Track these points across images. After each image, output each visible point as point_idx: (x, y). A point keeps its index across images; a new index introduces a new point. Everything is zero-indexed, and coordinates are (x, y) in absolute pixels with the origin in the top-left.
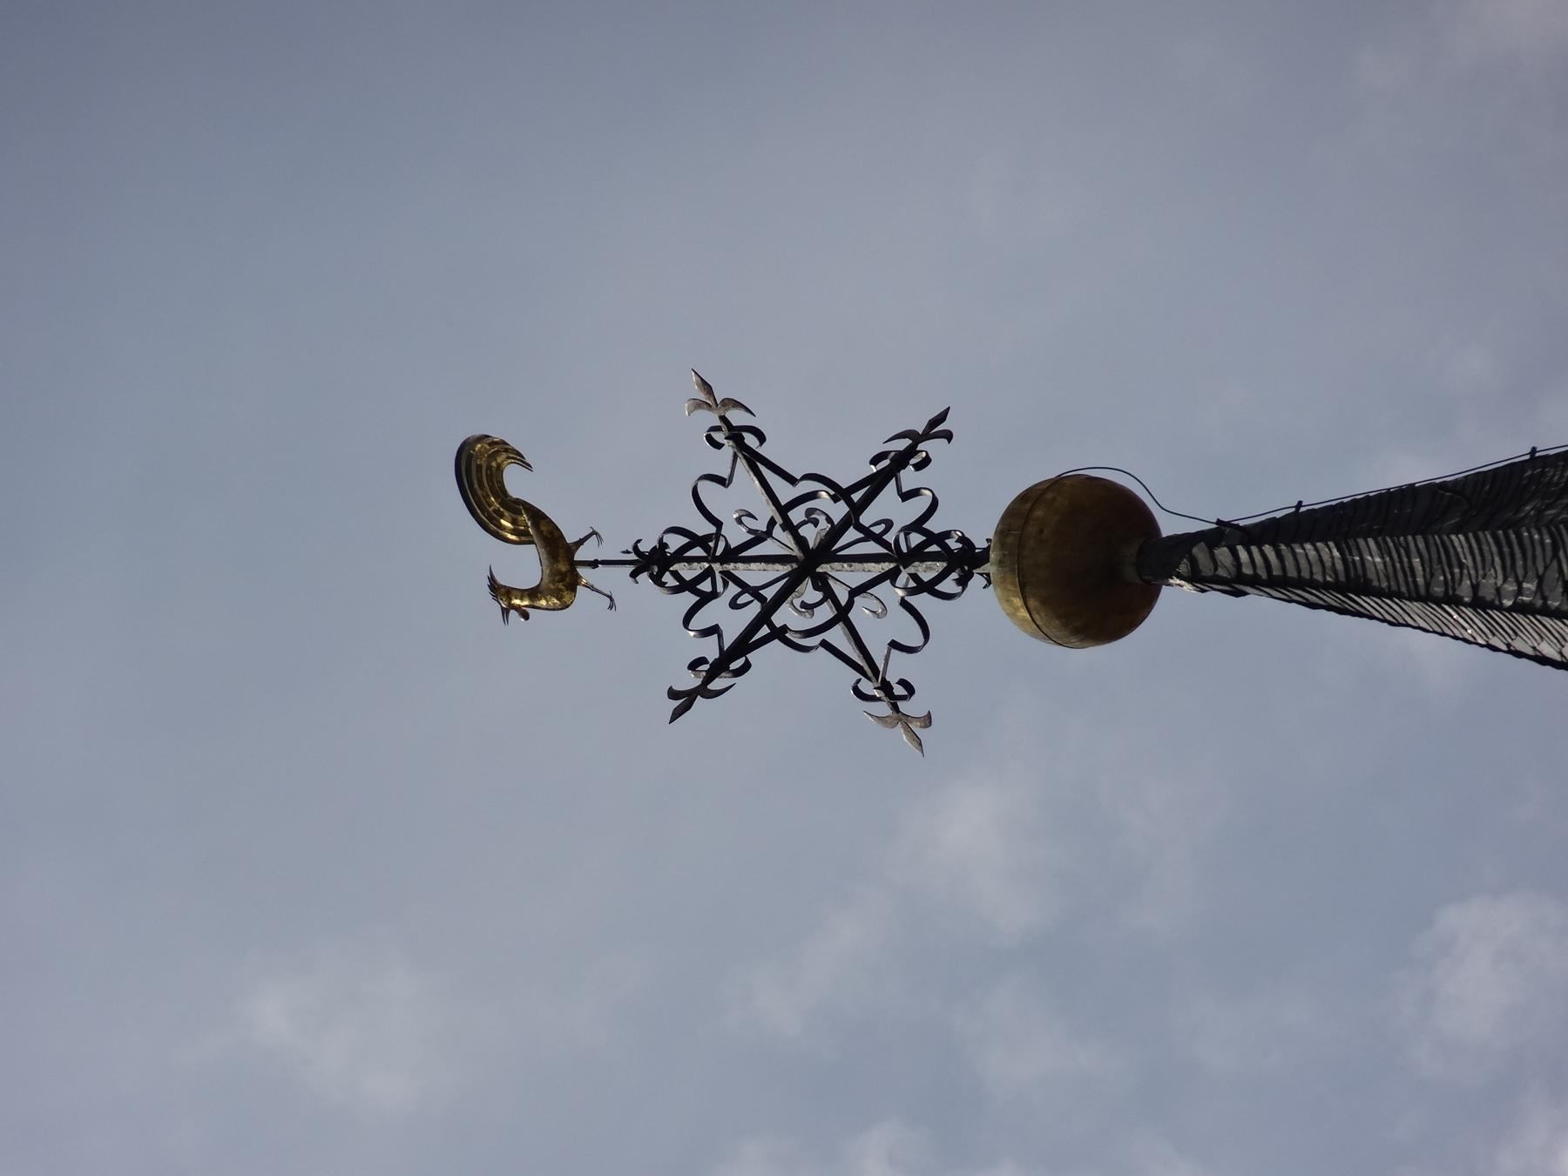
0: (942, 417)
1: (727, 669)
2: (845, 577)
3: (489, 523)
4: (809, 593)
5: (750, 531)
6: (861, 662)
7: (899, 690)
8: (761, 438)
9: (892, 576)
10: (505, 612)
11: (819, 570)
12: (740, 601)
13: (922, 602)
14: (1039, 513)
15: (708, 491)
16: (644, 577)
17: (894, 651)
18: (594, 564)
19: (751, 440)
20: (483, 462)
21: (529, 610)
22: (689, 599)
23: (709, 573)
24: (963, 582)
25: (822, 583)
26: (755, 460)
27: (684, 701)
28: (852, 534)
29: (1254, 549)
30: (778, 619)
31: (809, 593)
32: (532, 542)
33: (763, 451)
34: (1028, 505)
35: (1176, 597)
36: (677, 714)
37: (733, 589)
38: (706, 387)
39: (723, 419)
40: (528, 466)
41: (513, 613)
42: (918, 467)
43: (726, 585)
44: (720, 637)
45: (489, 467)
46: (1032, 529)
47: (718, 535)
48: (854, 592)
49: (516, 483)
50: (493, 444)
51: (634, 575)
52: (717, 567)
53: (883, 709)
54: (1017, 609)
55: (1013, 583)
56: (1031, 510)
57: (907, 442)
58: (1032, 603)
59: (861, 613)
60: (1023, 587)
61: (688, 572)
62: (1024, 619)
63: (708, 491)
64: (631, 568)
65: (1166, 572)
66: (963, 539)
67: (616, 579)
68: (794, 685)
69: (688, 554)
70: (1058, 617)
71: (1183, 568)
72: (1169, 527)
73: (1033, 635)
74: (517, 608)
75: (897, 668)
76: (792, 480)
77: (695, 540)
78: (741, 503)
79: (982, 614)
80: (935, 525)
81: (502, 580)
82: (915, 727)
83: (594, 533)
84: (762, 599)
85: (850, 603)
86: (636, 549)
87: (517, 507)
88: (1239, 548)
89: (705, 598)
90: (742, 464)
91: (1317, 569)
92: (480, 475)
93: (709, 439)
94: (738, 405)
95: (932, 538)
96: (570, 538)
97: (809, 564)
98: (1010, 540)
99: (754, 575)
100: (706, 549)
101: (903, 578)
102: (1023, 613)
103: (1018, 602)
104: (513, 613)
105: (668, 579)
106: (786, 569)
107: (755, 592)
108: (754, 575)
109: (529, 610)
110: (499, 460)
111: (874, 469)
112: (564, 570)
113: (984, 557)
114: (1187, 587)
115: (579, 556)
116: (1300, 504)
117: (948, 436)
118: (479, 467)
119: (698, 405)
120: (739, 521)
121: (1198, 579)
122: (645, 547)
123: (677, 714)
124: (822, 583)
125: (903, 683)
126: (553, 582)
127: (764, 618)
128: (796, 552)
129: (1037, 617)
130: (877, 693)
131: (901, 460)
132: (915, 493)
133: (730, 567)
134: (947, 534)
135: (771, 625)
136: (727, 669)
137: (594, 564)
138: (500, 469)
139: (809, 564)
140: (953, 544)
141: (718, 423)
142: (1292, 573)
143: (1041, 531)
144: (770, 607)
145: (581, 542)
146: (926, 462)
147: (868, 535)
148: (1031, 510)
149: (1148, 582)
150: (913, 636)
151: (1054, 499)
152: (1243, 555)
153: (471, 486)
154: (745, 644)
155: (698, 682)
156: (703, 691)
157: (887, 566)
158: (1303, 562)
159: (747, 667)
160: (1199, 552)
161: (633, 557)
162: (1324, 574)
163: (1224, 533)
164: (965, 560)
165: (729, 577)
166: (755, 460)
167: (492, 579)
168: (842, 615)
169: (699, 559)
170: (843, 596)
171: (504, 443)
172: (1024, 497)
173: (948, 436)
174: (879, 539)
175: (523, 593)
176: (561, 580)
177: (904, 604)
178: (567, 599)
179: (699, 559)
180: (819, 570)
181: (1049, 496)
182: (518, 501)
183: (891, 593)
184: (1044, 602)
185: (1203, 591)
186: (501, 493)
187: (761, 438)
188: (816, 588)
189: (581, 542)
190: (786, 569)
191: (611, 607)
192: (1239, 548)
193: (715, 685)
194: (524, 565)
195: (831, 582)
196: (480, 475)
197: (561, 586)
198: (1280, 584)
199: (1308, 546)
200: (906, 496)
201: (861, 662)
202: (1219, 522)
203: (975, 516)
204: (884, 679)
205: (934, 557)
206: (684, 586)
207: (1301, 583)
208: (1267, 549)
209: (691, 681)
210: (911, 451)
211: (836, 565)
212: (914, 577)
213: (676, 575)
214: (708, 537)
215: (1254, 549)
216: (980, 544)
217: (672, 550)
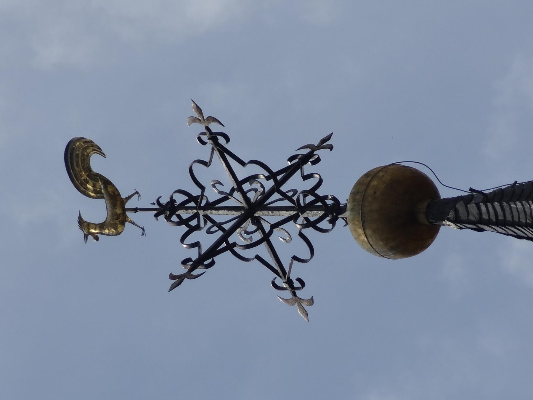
0: (328, 138)
1: (202, 264)
2: (269, 218)
3: (80, 186)
4: (249, 226)
5: (220, 192)
6: (277, 268)
7: (297, 284)
8: (227, 139)
9: (294, 218)
10: (86, 236)
11: (256, 215)
12: (212, 230)
13: (309, 232)
14: (374, 183)
15: (198, 169)
16: (162, 217)
17: (295, 262)
18: (136, 210)
19: (221, 140)
20: (79, 152)
21: (99, 235)
22: (184, 229)
23: (196, 216)
24: (333, 222)
25: (257, 221)
26: (223, 152)
27: (178, 280)
28: (276, 196)
29: (489, 205)
30: (231, 240)
31: (249, 226)
32: (103, 197)
33: (228, 147)
34: (369, 179)
35: (448, 231)
36: (173, 287)
37: (209, 224)
38: (199, 110)
39: (207, 128)
40: (103, 155)
41: (90, 237)
42: (314, 163)
43: (206, 223)
44: (200, 248)
45: (83, 155)
46: (370, 191)
47: (202, 195)
48: (274, 226)
49: (96, 164)
50: (86, 142)
51: (156, 216)
52: (201, 212)
53: (288, 294)
54: (359, 235)
55: (358, 221)
56: (370, 181)
57: (309, 150)
58: (368, 232)
59: (277, 238)
60: (363, 222)
61: (185, 214)
62: (364, 241)
63: (198, 169)
64: (155, 212)
65: (443, 217)
66: (334, 199)
67: (146, 219)
68: (238, 277)
69: (187, 205)
70: (382, 240)
71: (451, 215)
72: (445, 193)
73: (368, 250)
74: (92, 234)
75: (297, 272)
76: (243, 164)
77: (191, 198)
78: (216, 177)
79: (343, 243)
80: (320, 192)
81: (85, 218)
82: (305, 305)
83: (137, 192)
84: (223, 230)
85: (271, 232)
86: (158, 201)
87: (96, 177)
88: (481, 204)
89: (192, 229)
90: (216, 154)
91: (522, 216)
92: (77, 158)
93: (200, 139)
94: (215, 120)
95: (319, 199)
96: (124, 196)
97: (251, 211)
98: (358, 197)
99: (219, 216)
100: (196, 203)
101: (301, 220)
102: (363, 237)
103: (361, 231)
104: (90, 237)
105: (174, 218)
106: (238, 214)
107: (220, 226)
108: (219, 216)
109: (99, 235)
110: (88, 151)
111: (289, 164)
112: (119, 212)
113: (343, 210)
114: (453, 226)
115: (128, 205)
116: (516, 182)
117: (331, 148)
118: (77, 155)
119: (194, 120)
120: (214, 186)
121: (457, 221)
122: (164, 201)
123: (173, 287)
124: (257, 221)
125: (299, 280)
126: (113, 219)
127: (224, 239)
128: (244, 205)
129: (370, 240)
130: (285, 286)
131: (305, 159)
132: (310, 176)
133: (208, 212)
134: (326, 197)
135: (227, 243)
136: (202, 264)
137: (136, 210)
138: (88, 156)
139: (251, 211)
140: (329, 202)
141: (204, 130)
142: (509, 218)
143: (375, 193)
144: (228, 233)
145: (129, 198)
146: (318, 160)
147: (285, 196)
148: (370, 181)
149: (432, 223)
150: (305, 253)
151: (383, 176)
152: (483, 208)
153: (72, 165)
154: (214, 251)
155: (186, 271)
156: (189, 275)
157: (292, 213)
158: (515, 213)
159: (213, 263)
160: (460, 207)
161: (157, 206)
162: (526, 218)
163: (475, 197)
164: (334, 210)
165: (207, 218)
166: (223, 152)
167: (80, 218)
168: (266, 238)
169: (192, 208)
170: (267, 229)
171: (92, 142)
172: (367, 175)
173: (331, 148)
174: (290, 199)
175: (96, 226)
176: (117, 219)
177: (301, 235)
178: (120, 230)
179: (192, 208)
180: (256, 215)
181: (381, 174)
182: (97, 175)
183: (294, 227)
184: (374, 231)
185: (461, 228)
186: (88, 169)
187: (227, 139)
188: (253, 223)
189: (129, 198)
190: (238, 214)
191: (143, 235)
192: (481, 204)
193: (196, 272)
194: (97, 210)
195: (262, 222)
196: (77, 158)
197: (117, 222)
198: (502, 224)
199: (518, 203)
200: (306, 178)
201: (277, 268)
202: (471, 190)
203: (338, 179)
204: (289, 278)
205: (318, 208)
206: (182, 222)
207: (513, 224)
208: (496, 204)
209: (183, 270)
210: (311, 155)
211: (265, 212)
212: (306, 219)
213: (179, 216)
214: (197, 197)
215: (489, 205)
216: (343, 200)
217: (178, 203)
